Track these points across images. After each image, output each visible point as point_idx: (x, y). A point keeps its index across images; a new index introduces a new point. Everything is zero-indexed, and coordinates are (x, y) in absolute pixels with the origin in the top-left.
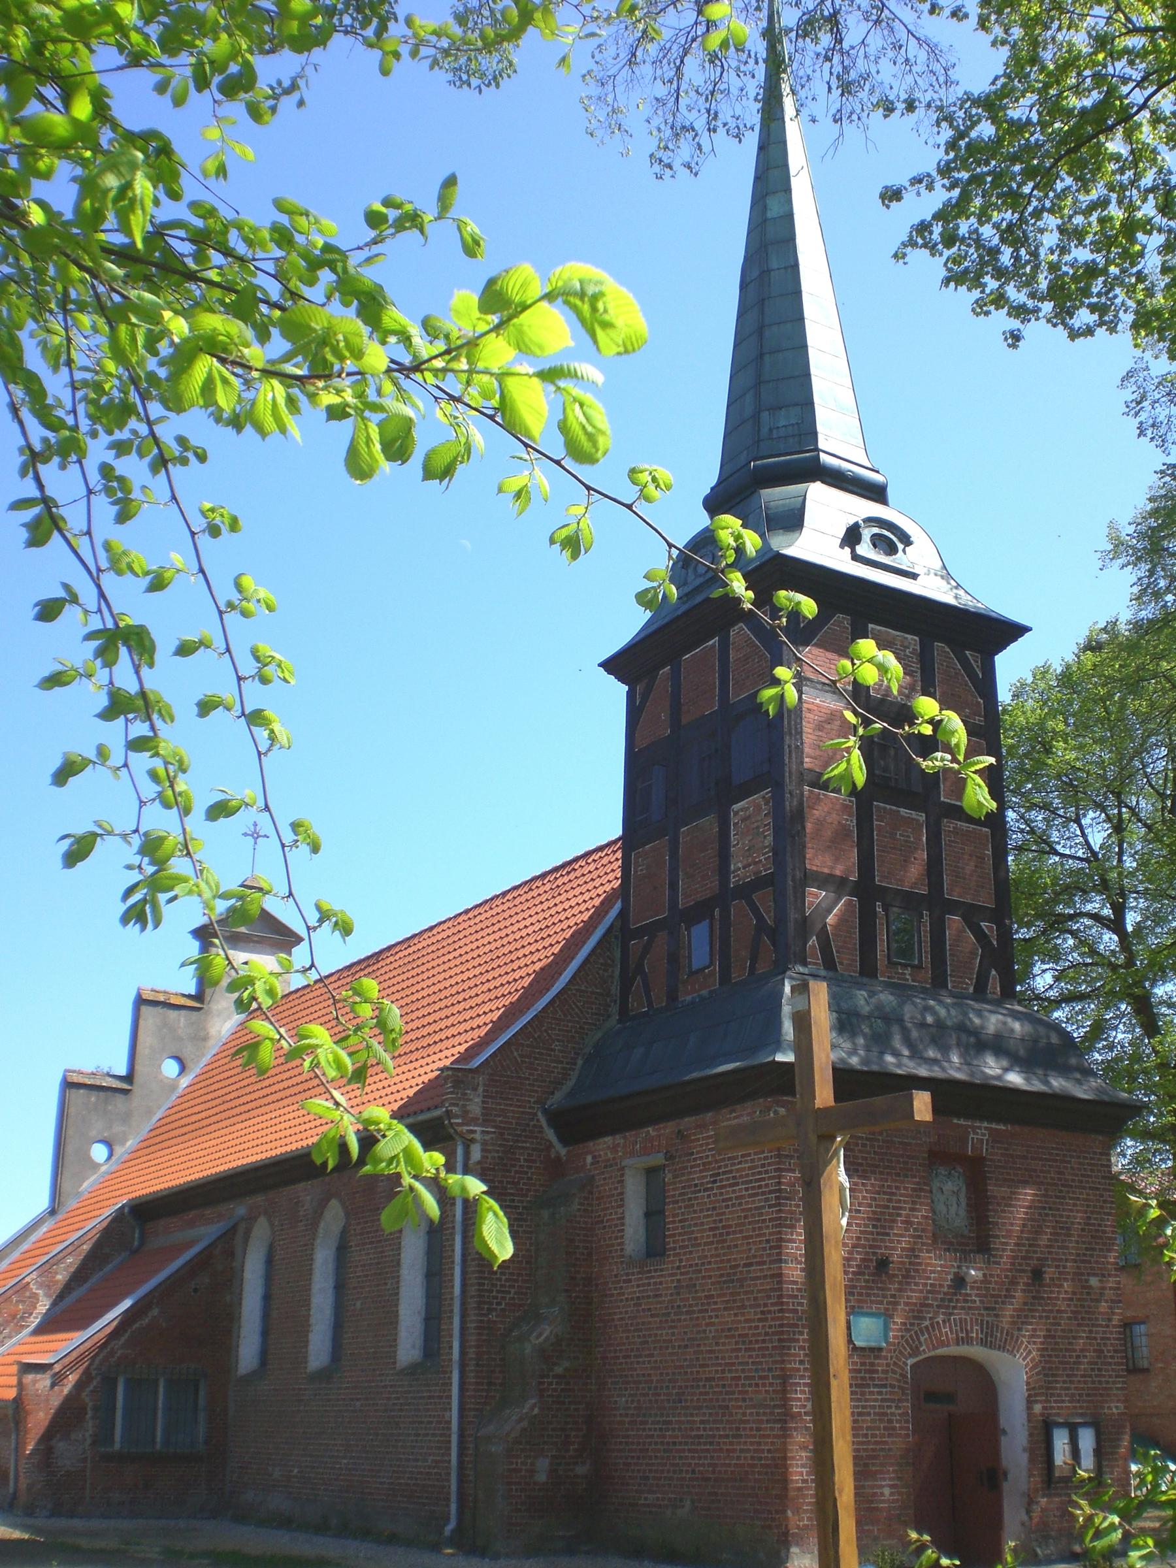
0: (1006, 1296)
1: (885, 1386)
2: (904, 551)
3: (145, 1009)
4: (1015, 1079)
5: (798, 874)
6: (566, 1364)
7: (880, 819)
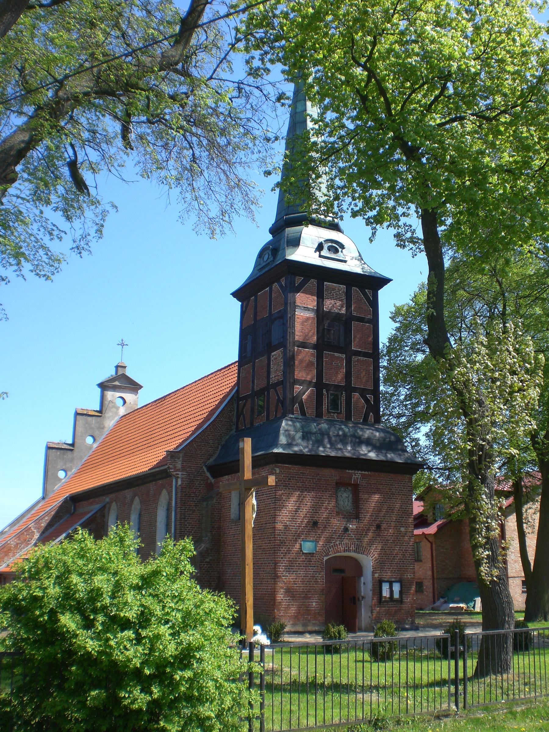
2: (342, 252)
3: (78, 416)
4: (372, 455)
5: (292, 381)
6: (211, 558)
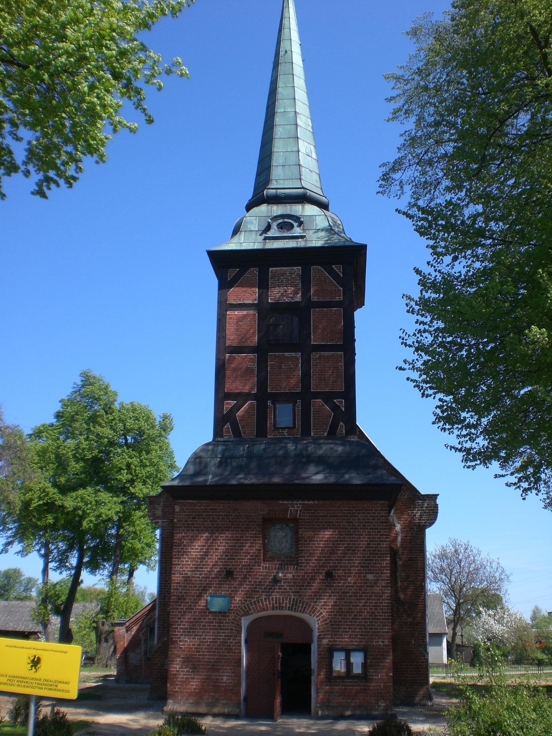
0: (307, 586)
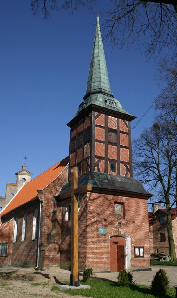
1: (105, 240)
3: (8, 186)
7: (109, 147)
